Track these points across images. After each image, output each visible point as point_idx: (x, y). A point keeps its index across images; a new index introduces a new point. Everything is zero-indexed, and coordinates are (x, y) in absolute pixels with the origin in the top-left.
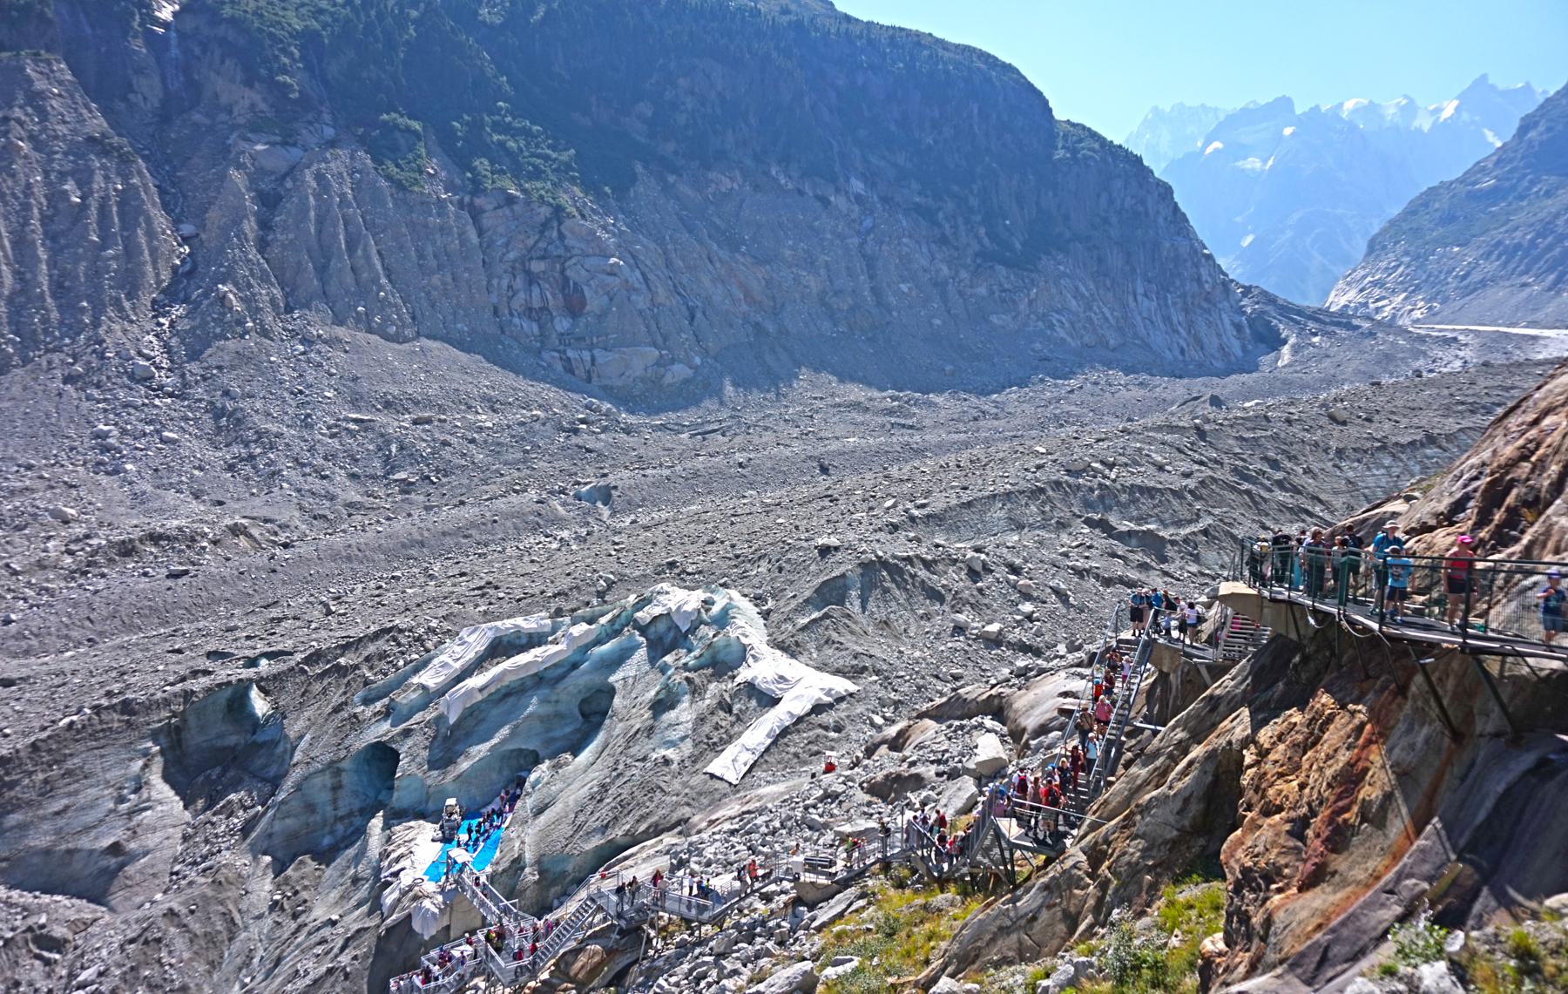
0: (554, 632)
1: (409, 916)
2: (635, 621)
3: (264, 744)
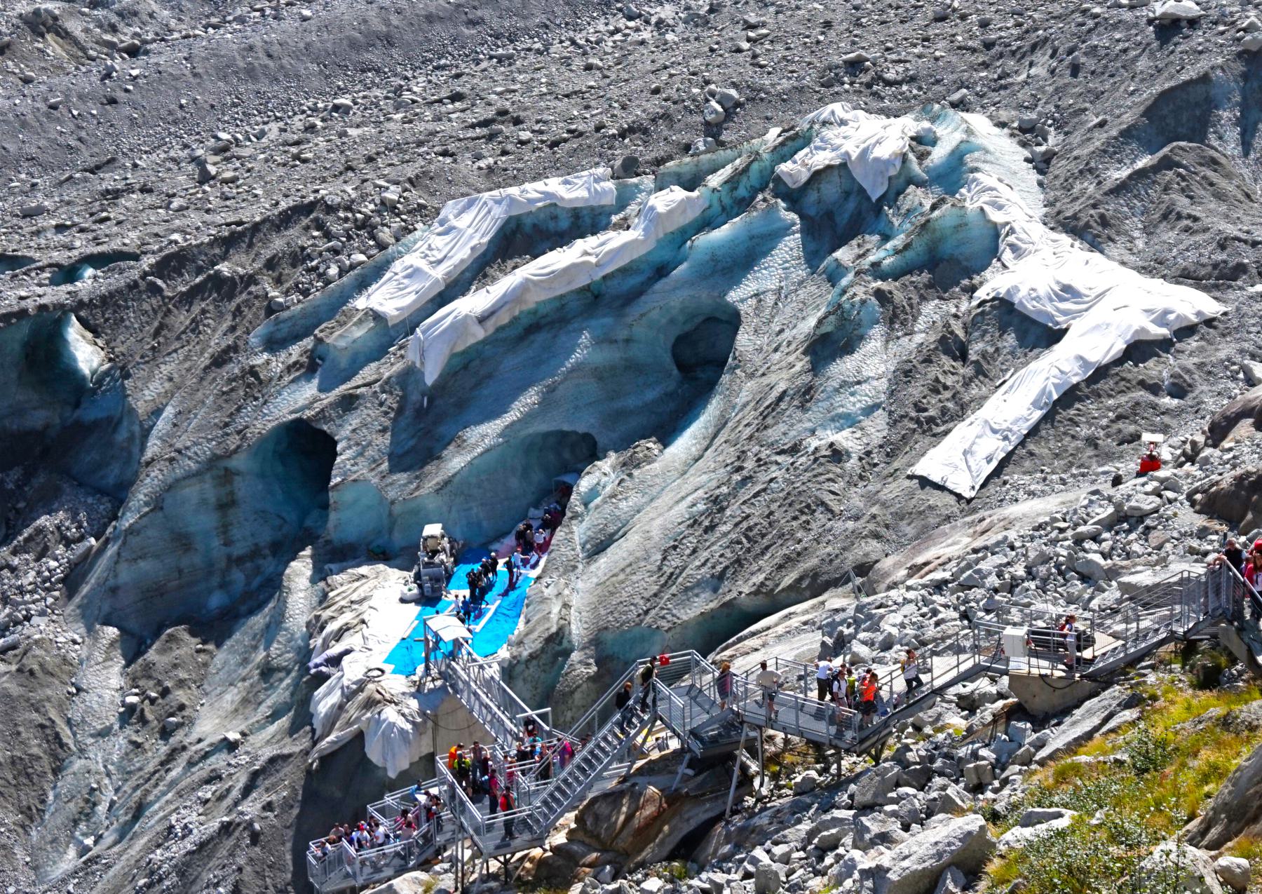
0: (622, 204)
1: (360, 737)
2: (778, 180)
3: (96, 424)
